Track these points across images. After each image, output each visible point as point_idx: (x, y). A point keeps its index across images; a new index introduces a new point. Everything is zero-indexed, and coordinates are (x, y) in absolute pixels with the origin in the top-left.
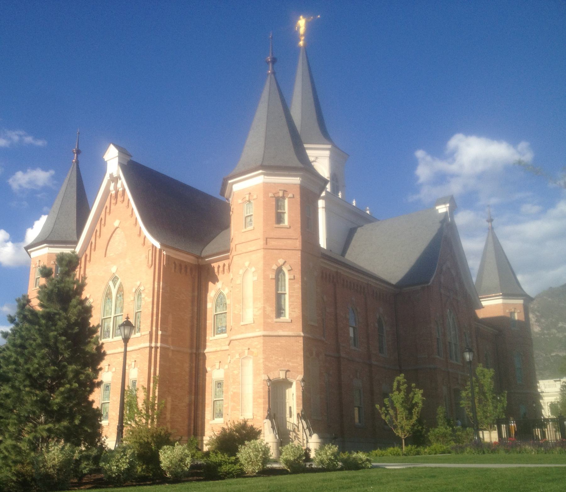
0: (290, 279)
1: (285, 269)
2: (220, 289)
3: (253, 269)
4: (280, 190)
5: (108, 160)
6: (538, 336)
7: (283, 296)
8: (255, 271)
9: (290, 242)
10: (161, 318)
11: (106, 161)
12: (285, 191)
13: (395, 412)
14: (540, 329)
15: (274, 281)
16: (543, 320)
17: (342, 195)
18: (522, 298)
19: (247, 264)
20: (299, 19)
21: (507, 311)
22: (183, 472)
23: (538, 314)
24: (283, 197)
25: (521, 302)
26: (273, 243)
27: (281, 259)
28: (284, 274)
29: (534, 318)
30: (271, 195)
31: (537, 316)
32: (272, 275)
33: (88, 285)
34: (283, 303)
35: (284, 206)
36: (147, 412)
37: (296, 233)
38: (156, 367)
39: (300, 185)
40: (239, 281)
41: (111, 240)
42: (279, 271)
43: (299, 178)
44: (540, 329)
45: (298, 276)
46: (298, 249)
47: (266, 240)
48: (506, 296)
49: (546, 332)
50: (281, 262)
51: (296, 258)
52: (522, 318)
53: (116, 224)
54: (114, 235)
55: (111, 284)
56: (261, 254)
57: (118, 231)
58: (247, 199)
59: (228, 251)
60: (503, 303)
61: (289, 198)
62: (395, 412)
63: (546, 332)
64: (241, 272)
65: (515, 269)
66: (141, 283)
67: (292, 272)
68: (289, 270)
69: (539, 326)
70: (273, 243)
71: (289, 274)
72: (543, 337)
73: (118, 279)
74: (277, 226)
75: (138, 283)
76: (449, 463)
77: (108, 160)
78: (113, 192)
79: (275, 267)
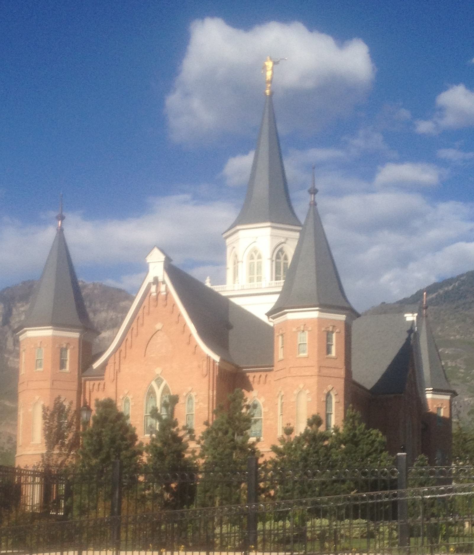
0: (336, 402)
1: (333, 394)
2: (255, 397)
3: (307, 391)
4: (331, 326)
5: (151, 263)
7: (329, 416)
8: (309, 393)
9: (336, 371)
11: (149, 263)
12: (334, 326)
15: (325, 403)
18: (344, 312)
19: (301, 386)
21: (435, 406)
22: (436, 526)
24: (332, 332)
25: (342, 317)
26: (325, 371)
27: (330, 385)
28: (331, 398)
30: (323, 329)
32: (324, 399)
34: (329, 422)
35: (332, 339)
36: (98, 498)
37: (341, 363)
39: (345, 321)
40: (293, 400)
41: (151, 341)
42: (328, 395)
43: (344, 316)
45: (342, 400)
46: (342, 377)
47: (320, 367)
48: (325, 307)
50: (330, 387)
51: (340, 384)
52: (447, 415)
53: (159, 326)
54: (154, 336)
55: (154, 384)
56: (315, 380)
57: (160, 334)
58: (302, 329)
59: (273, 366)
60: (432, 398)
61: (337, 332)
64: (296, 392)
65: (331, 245)
66: (193, 388)
67: (337, 396)
68: (336, 395)
70: (325, 371)
71: (336, 398)
73: (162, 381)
74: (326, 356)
75: (190, 389)
77: (151, 263)
78: (154, 294)
79: (325, 392)
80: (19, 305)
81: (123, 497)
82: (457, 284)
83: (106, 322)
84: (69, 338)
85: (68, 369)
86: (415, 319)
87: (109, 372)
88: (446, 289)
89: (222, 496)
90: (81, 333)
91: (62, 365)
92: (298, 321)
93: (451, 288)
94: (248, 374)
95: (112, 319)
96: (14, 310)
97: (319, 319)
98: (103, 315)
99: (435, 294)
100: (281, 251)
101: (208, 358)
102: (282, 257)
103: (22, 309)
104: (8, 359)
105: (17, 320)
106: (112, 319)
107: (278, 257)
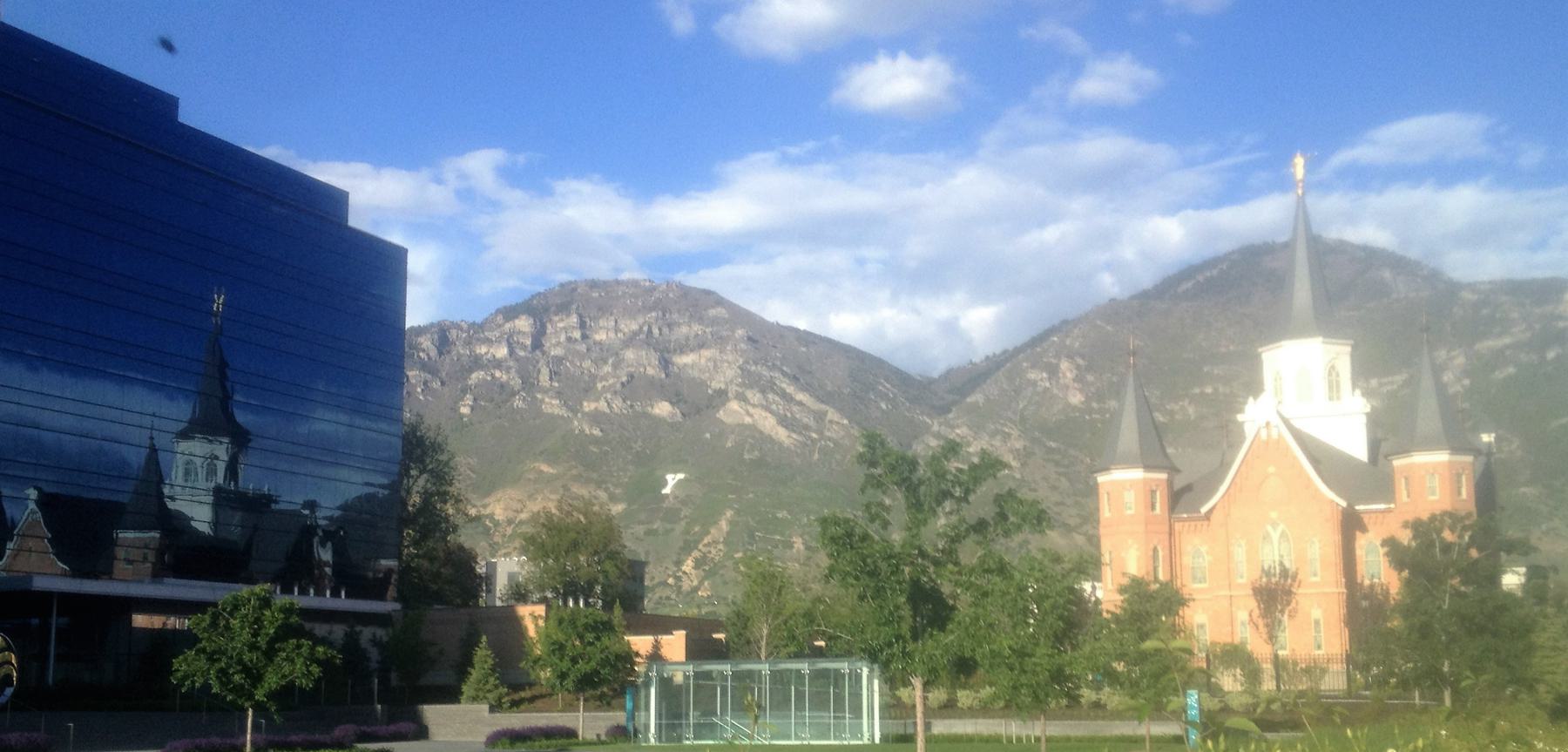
6: (1077, 414)
10: (251, 741)
13: (527, 688)
14: (1083, 399)
16: (1090, 378)
17: (1346, 733)
20: (1481, 438)
23: (1080, 361)
29: (1071, 371)
30: (1454, 472)
31: (1078, 367)
33: (182, 104)
38: (873, 719)
44: (1083, 399)
49: (1095, 405)
62: (527, 688)
63: (1095, 405)
69: (1081, 391)
72: (1087, 417)
76: (1336, 494)
80: (556, 318)
81: (474, 565)
82: (1225, 267)
83: (687, 339)
84: (1158, 480)
85: (1158, 510)
86: (1493, 439)
87: (1215, 516)
88: (1208, 274)
89: (328, 536)
90: (1168, 473)
91: (1153, 507)
92: (1426, 464)
93: (1215, 272)
94: (1362, 515)
95: (697, 335)
96: (549, 326)
97: (1450, 462)
98: (684, 330)
99: (1192, 282)
100: (1333, 367)
101: (1332, 501)
102: (1334, 374)
103: (561, 325)
104: (542, 401)
105: (554, 342)
106: (697, 335)
107: (1330, 374)
